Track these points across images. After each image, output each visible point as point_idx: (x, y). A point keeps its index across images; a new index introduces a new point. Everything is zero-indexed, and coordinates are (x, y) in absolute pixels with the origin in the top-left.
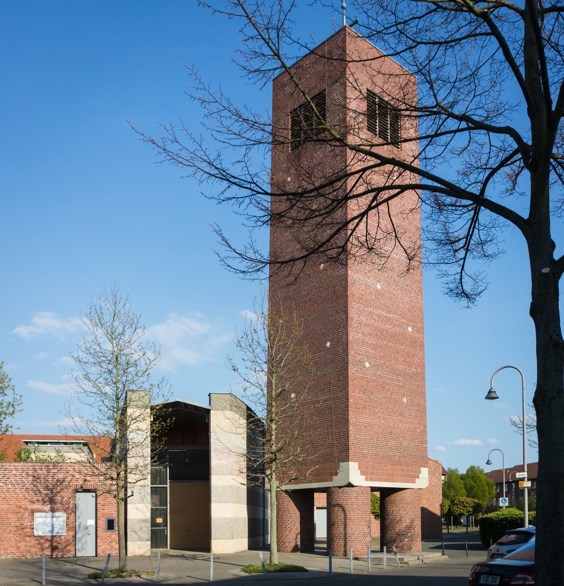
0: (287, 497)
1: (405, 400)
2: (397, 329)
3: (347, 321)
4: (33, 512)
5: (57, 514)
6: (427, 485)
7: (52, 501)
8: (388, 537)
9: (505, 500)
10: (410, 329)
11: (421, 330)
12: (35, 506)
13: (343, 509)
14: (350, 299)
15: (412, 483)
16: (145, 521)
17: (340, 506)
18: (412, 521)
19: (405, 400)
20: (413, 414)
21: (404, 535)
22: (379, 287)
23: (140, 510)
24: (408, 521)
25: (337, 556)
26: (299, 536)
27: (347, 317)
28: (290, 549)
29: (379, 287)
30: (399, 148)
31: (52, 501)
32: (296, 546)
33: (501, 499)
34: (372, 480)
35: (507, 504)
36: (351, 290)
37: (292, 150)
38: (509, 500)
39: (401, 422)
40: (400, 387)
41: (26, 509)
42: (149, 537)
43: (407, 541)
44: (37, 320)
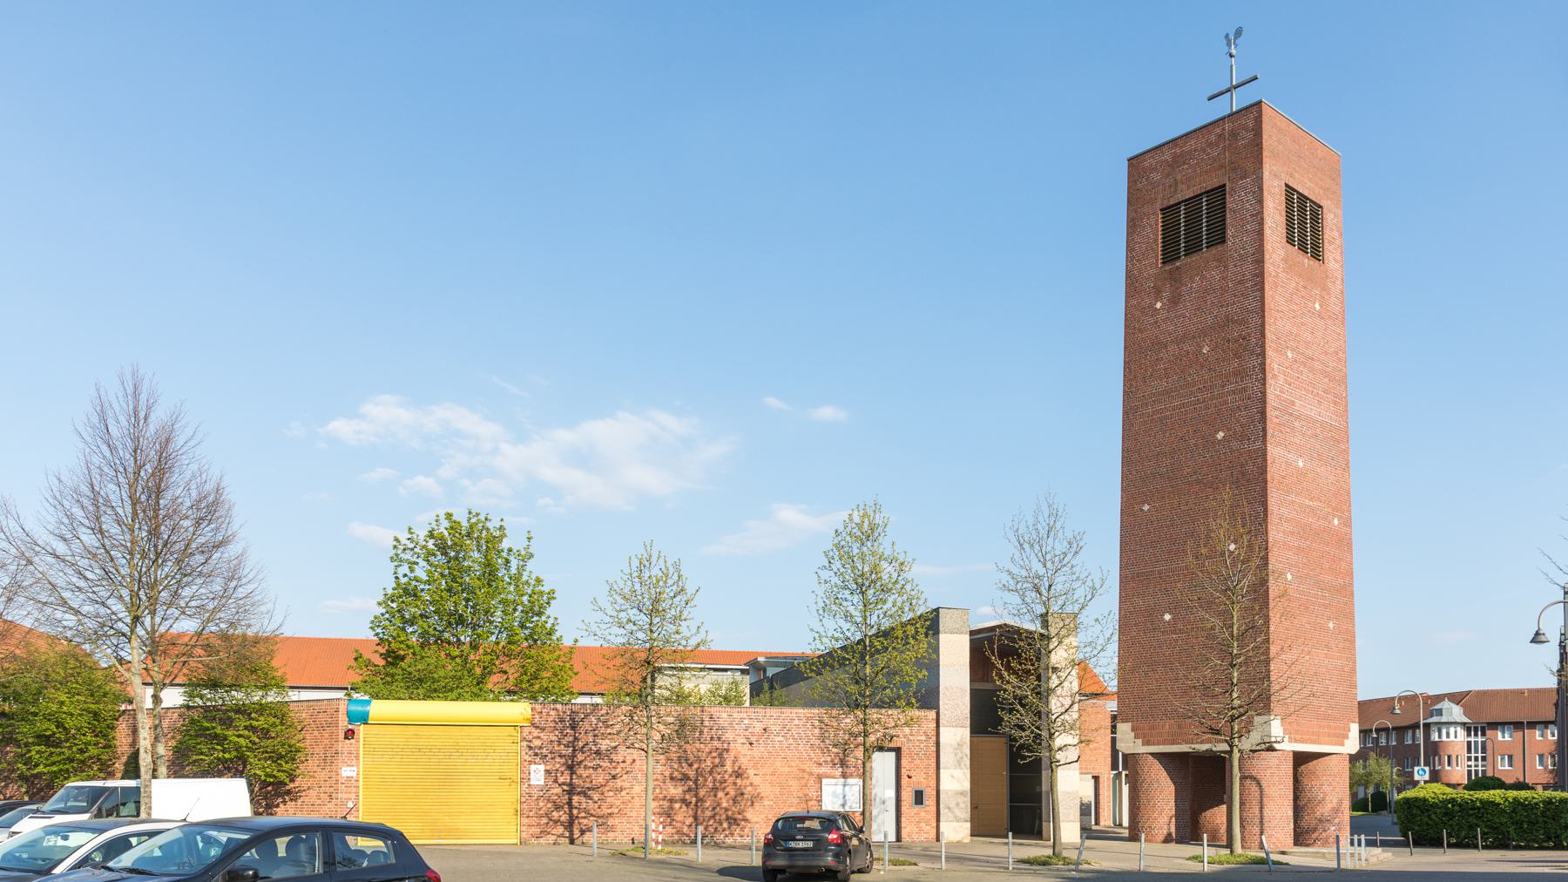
3: (1266, 515)
4: (820, 778)
5: (850, 781)
6: (567, 642)
7: (843, 763)
8: (1303, 824)
10: (1336, 522)
11: (1347, 523)
12: (823, 770)
16: (962, 793)
17: (1253, 778)
18: (1340, 802)
22: (1301, 464)
23: (956, 780)
27: (1266, 510)
28: (1162, 838)
29: (1301, 464)
31: (843, 763)
32: (1169, 834)
34: (1296, 741)
35: (1427, 777)
36: (1273, 472)
40: (1326, 606)
41: (811, 774)
42: (968, 816)
44: (370, 409)
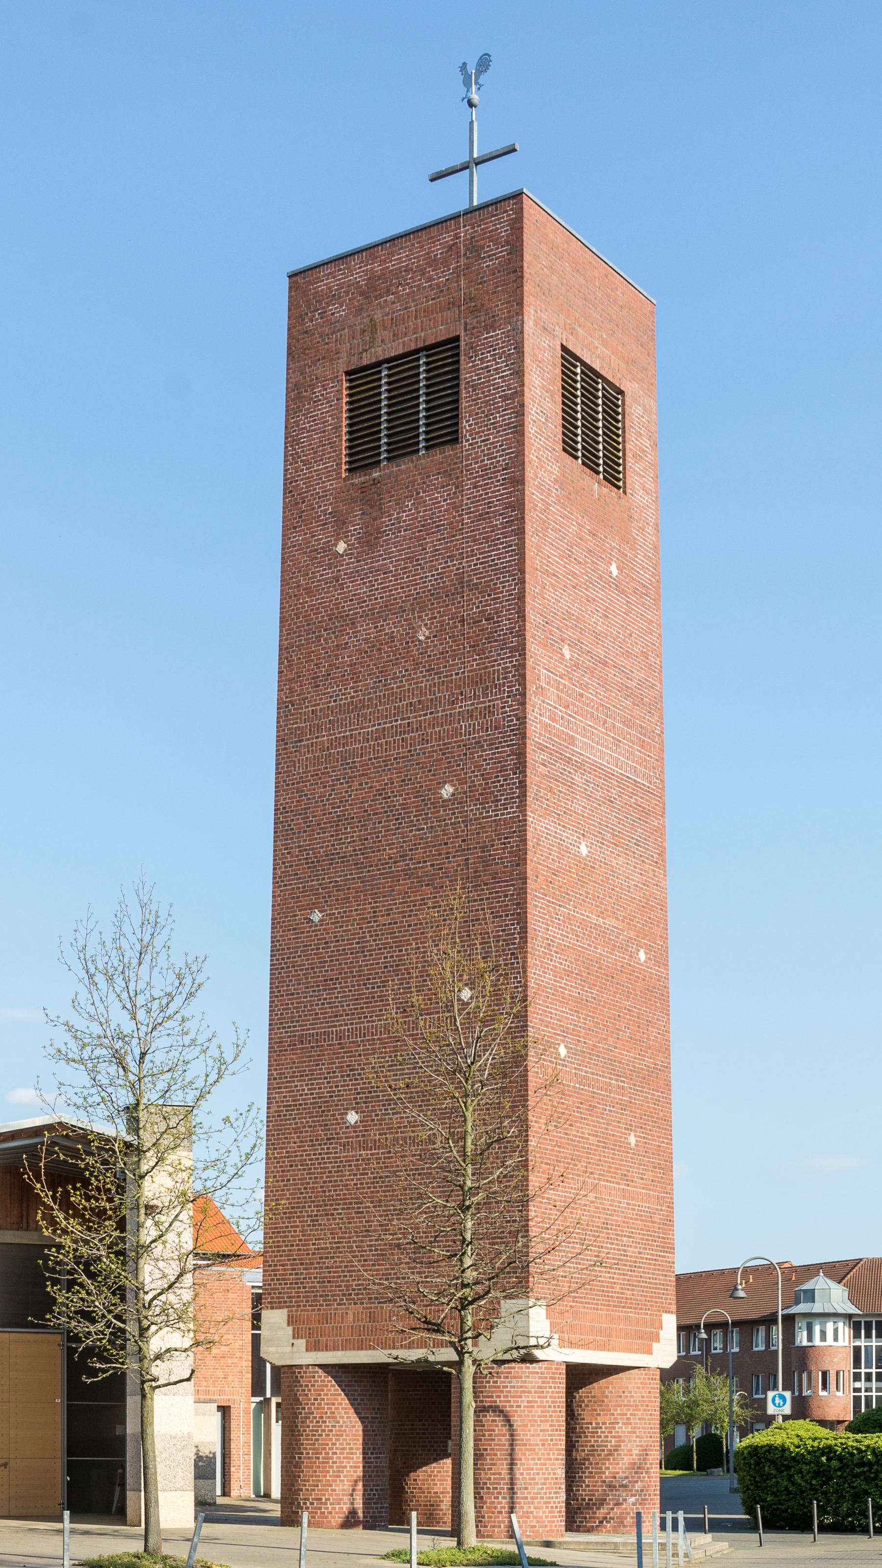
0: (330, 1381)
1: (632, 1140)
2: (618, 955)
3: (524, 939)
9: (783, 1398)
10: (642, 956)
11: (661, 958)
13: (508, 1421)
14: (531, 885)
15: (644, 1353)
17: (498, 1410)
19: (632, 1140)
20: (649, 1175)
21: (625, 1486)
24: (635, 1451)
25: (488, 1536)
26: (360, 1486)
27: (524, 931)
28: (339, 1519)
29: (584, 850)
30: (618, 488)
32: (353, 1513)
33: (771, 1394)
34: (572, 1345)
35: (787, 1410)
36: (538, 862)
37: (350, 470)
38: (793, 1399)
39: (624, 1197)
43: (634, 1504)
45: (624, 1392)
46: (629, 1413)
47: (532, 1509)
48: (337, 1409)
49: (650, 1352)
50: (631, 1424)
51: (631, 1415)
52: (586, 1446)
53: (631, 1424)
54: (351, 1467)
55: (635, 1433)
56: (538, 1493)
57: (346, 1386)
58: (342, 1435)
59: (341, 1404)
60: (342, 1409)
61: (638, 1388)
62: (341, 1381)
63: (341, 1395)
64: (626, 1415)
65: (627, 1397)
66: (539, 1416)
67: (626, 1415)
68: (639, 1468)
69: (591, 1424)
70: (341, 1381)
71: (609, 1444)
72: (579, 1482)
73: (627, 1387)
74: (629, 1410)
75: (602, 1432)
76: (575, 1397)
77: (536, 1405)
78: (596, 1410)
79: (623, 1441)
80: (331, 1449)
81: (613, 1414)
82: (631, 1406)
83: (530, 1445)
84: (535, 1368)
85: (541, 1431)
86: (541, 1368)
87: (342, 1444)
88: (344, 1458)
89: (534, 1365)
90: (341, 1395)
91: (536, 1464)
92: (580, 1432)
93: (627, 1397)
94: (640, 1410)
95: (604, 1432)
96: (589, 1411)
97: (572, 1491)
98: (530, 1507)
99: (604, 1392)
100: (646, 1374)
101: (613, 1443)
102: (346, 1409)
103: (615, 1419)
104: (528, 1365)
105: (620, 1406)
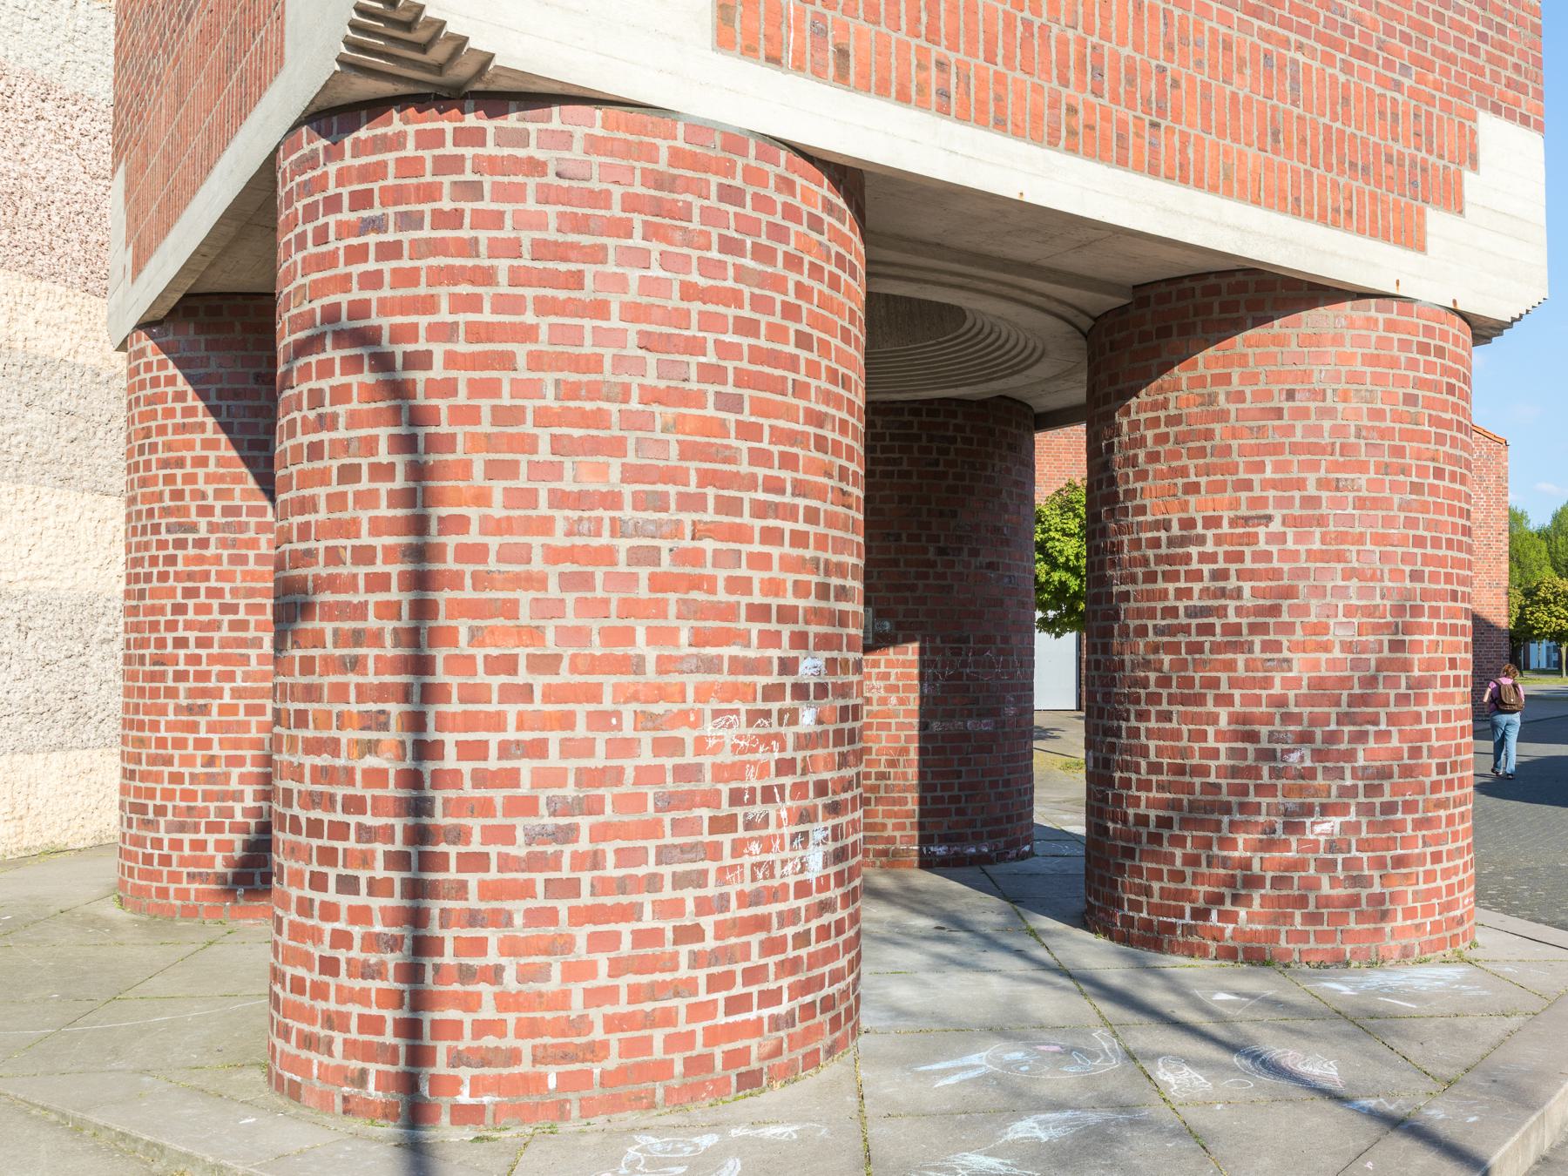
45: (1291, 395)
46: (1311, 478)
47: (492, 957)
48: (190, 479)
49: (1411, 237)
50: (1321, 521)
51: (1322, 484)
52: (1151, 613)
53: (1321, 521)
54: (237, 693)
55: (1340, 557)
56: (535, 862)
57: (221, 395)
58: (206, 576)
59: (201, 462)
60: (209, 479)
61: (1355, 378)
62: (207, 379)
63: (202, 427)
64: (1300, 484)
65: (1303, 413)
66: (544, 418)
67: (1300, 484)
68: (1362, 700)
69: (1166, 526)
70: (207, 379)
71: (1232, 604)
72: (1129, 750)
73: (1306, 376)
74: (1315, 466)
75: (1204, 558)
76: (1117, 431)
77: (521, 351)
78: (1183, 472)
79: (1289, 593)
80: (172, 626)
81: (1247, 485)
82: (1322, 450)
83: (480, 581)
84: (521, 139)
85: (560, 499)
86: (565, 140)
87: (207, 609)
88: (212, 659)
89: (512, 120)
90: (202, 427)
91: (526, 693)
92: (1133, 562)
93: (1303, 413)
94: (1362, 467)
95: (1212, 558)
96: (1160, 475)
97: (1110, 782)
98: (479, 946)
99: (1211, 399)
100: (1391, 326)
101: (1248, 601)
102: (221, 478)
103: (1255, 502)
104: (471, 120)
105: (1276, 449)
